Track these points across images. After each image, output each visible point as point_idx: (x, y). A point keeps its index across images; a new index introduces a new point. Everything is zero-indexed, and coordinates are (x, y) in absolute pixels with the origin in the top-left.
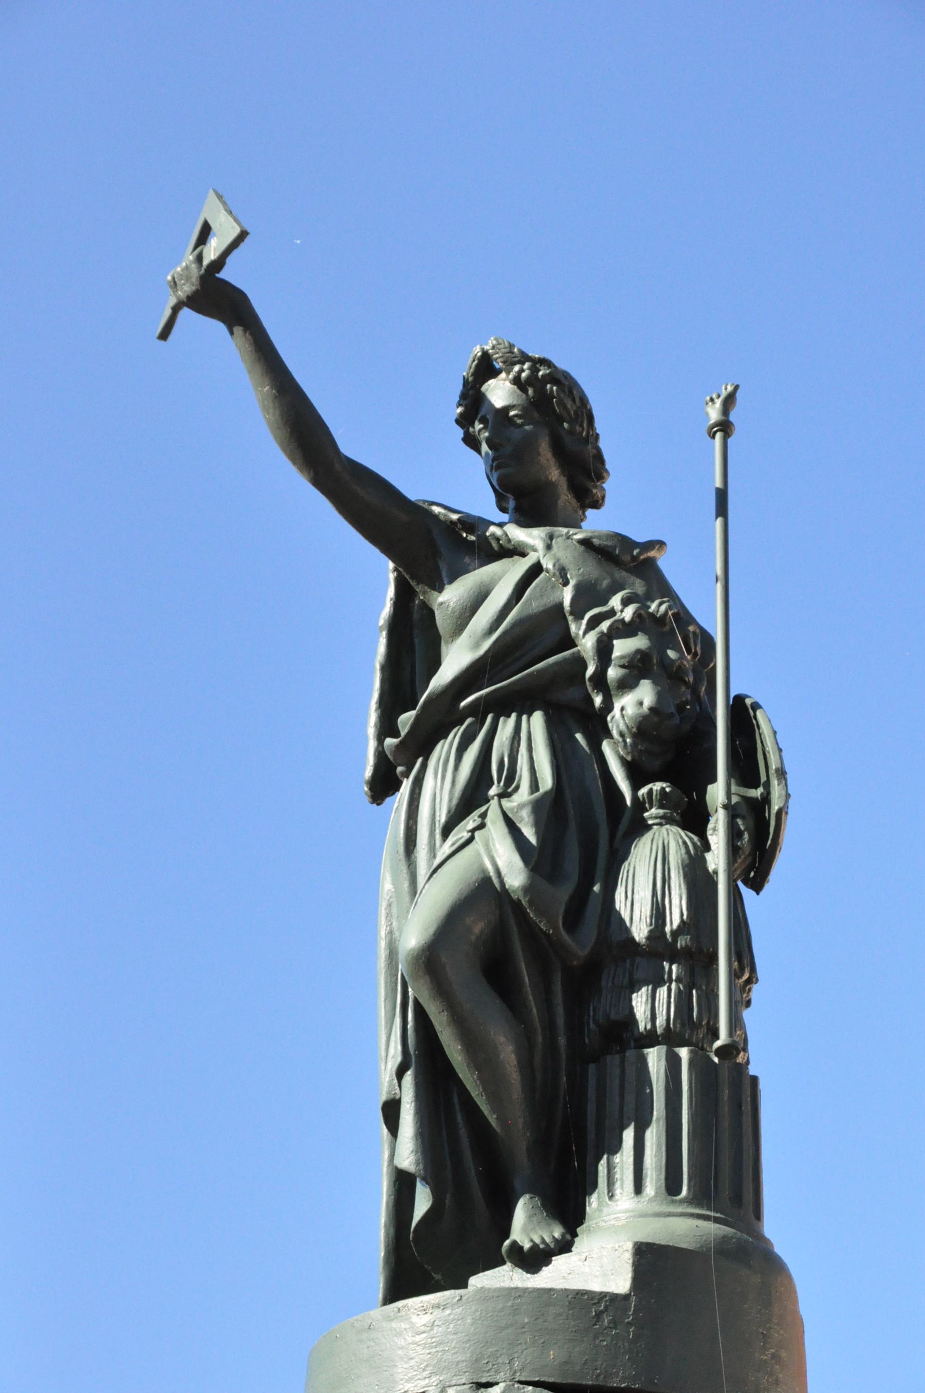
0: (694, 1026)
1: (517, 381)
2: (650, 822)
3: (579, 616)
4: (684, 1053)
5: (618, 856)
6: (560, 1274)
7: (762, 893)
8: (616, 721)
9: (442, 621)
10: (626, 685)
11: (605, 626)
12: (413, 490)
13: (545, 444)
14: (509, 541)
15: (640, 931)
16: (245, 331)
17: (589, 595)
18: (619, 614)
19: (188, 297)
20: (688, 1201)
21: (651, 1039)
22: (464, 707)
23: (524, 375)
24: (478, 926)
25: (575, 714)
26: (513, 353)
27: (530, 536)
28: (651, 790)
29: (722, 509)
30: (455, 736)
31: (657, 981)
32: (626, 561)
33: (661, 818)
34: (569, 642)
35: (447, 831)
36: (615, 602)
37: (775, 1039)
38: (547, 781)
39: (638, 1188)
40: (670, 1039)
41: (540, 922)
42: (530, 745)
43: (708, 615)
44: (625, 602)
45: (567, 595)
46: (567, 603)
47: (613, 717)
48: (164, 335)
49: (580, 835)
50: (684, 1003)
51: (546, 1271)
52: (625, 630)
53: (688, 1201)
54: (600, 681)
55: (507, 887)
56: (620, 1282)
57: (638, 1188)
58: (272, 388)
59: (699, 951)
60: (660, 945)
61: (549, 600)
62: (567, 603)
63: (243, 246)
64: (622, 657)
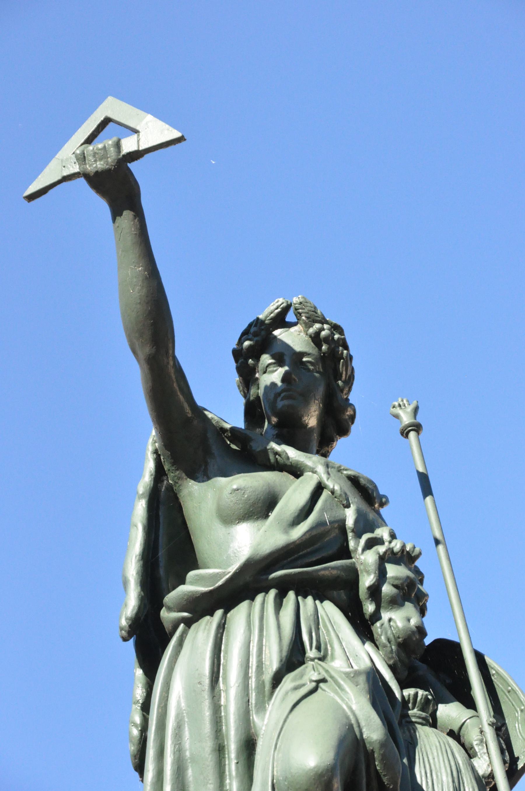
2: (414, 720)
3: (358, 535)
8: (385, 629)
13: (307, 395)
14: (288, 458)
16: (135, 217)
18: (387, 544)
19: (97, 173)
22: (273, 579)
23: (323, 333)
26: (316, 313)
28: (416, 695)
33: (423, 719)
34: (345, 553)
41: (384, 775)
46: (350, 522)
47: (382, 625)
55: (365, 736)
58: (145, 270)
62: (350, 522)
63: (178, 146)
64: (397, 578)
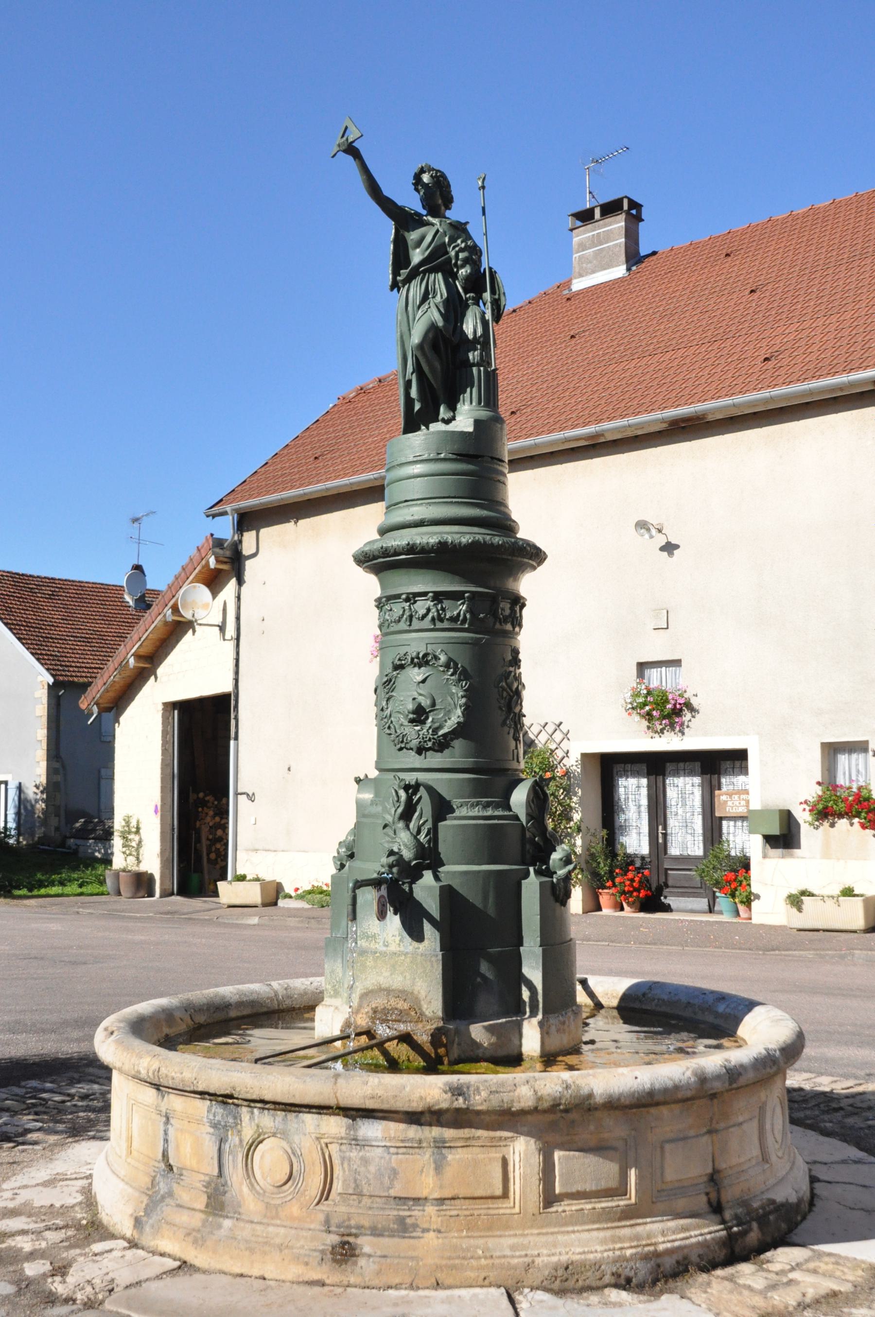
0: (484, 361)
1: (432, 176)
4: (482, 369)
5: (463, 315)
6: (452, 427)
7: (819, 745)
9: (410, 243)
10: (463, 266)
11: (457, 249)
12: (400, 202)
13: (437, 193)
15: (471, 336)
17: (453, 240)
20: (484, 406)
21: (473, 365)
24: (431, 335)
25: (450, 275)
27: (435, 221)
29: (484, 214)
30: (419, 278)
31: (475, 349)
32: (459, 229)
34: (447, 253)
35: (419, 307)
36: (459, 241)
37: (499, 359)
38: (445, 295)
39: (471, 403)
40: (478, 365)
42: (438, 280)
43: (481, 244)
44: (462, 242)
45: (447, 240)
48: (333, 157)
49: (454, 309)
50: (481, 354)
51: (451, 425)
52: (462, 250)
53: (484, 406)
54: (456, 265)
56: (471, 429)
57: (471, 403)
59: (484, 341)
60: (476, 340)
61: (442, 241)
